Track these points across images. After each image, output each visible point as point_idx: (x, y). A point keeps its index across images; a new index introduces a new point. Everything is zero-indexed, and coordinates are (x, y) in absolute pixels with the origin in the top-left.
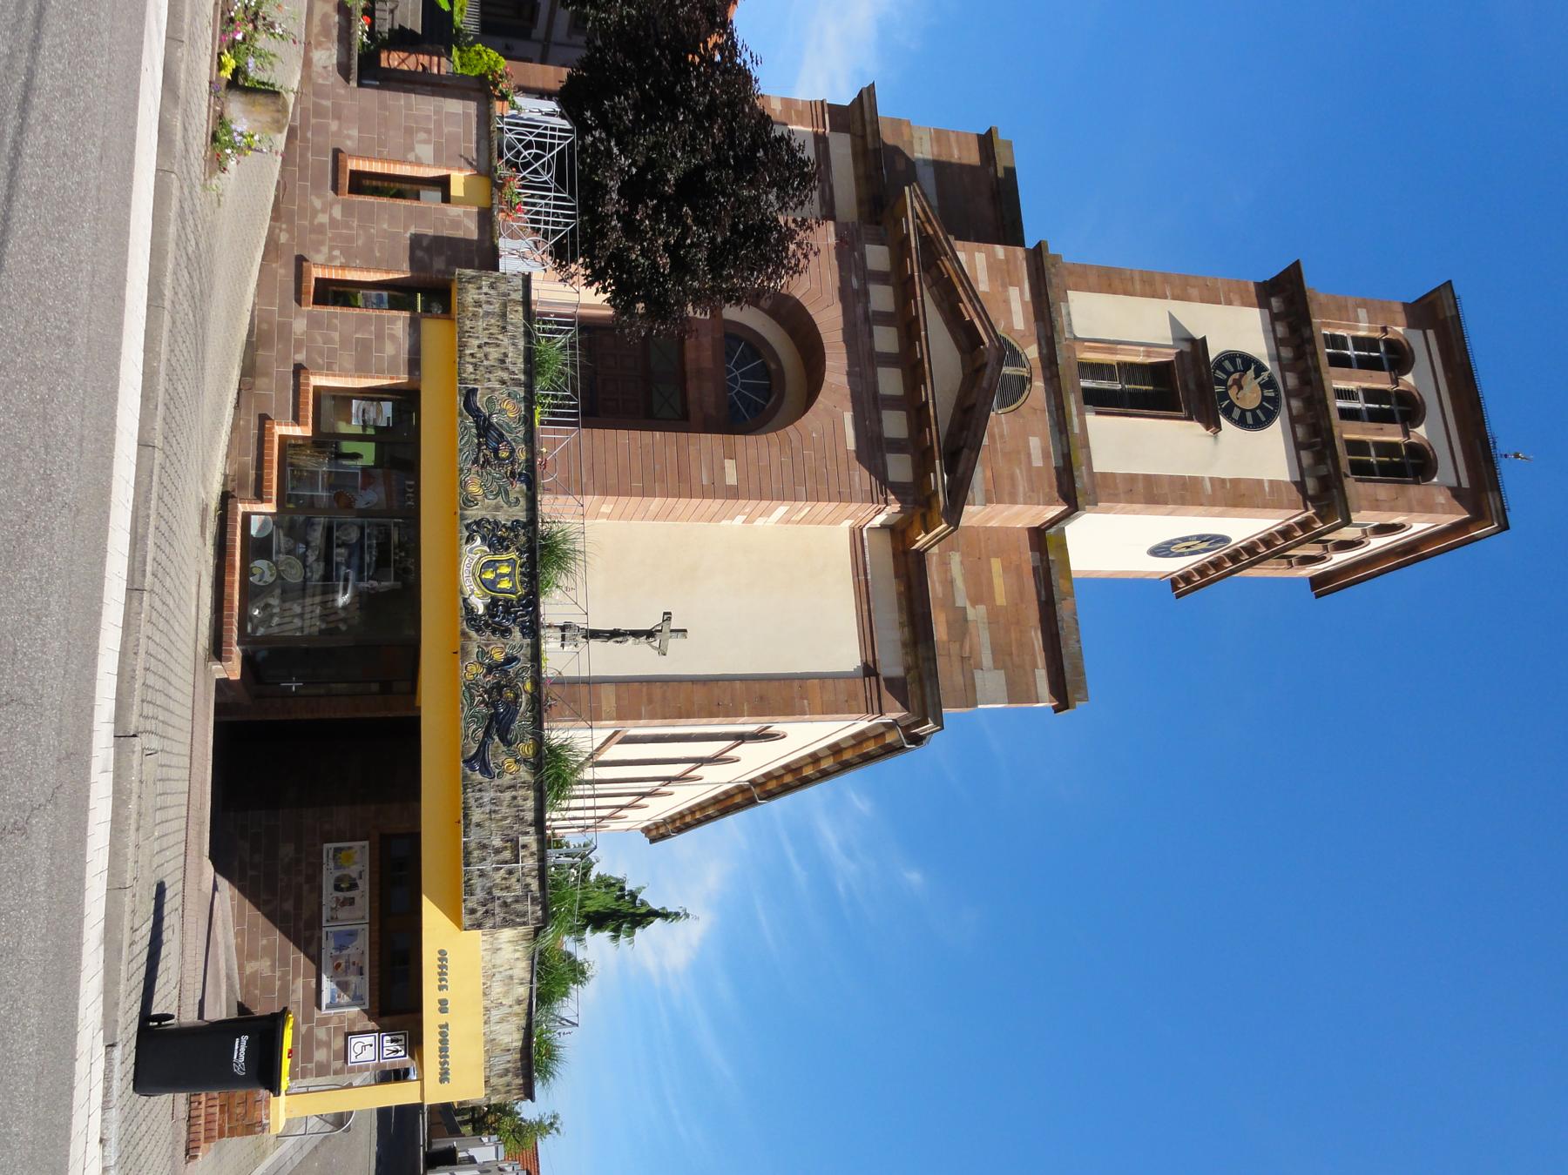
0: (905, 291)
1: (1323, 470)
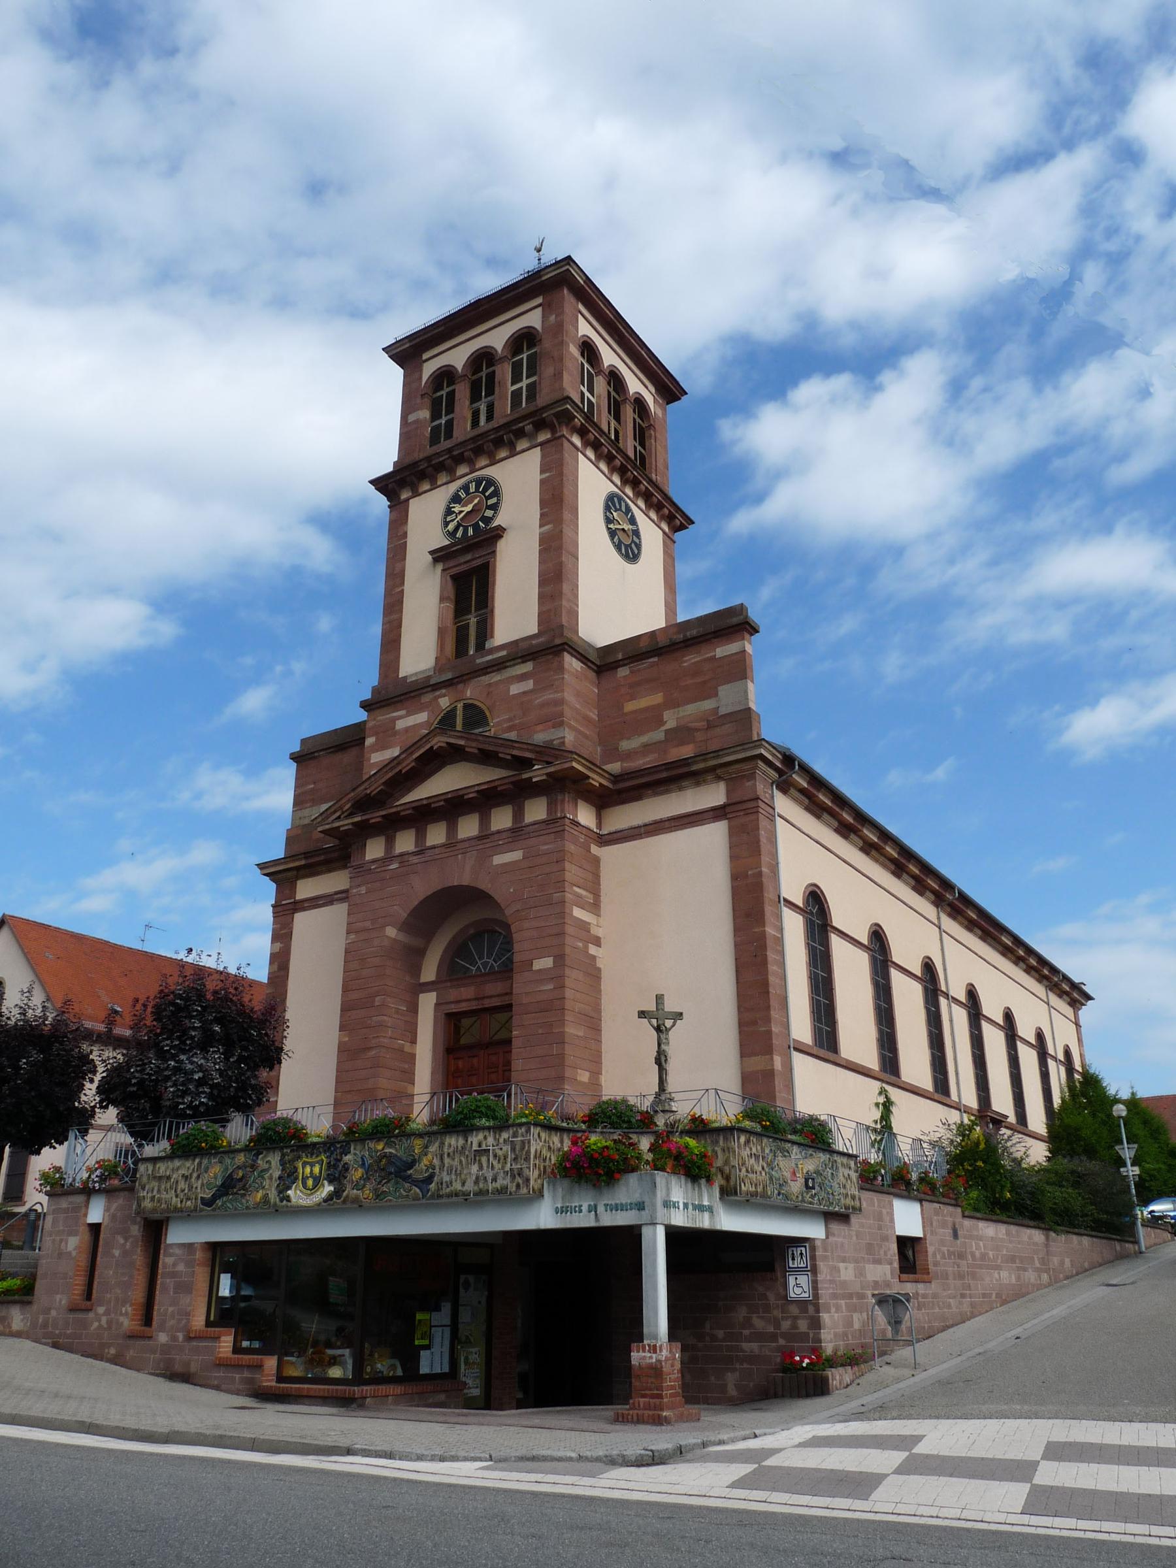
1: (529, 428)
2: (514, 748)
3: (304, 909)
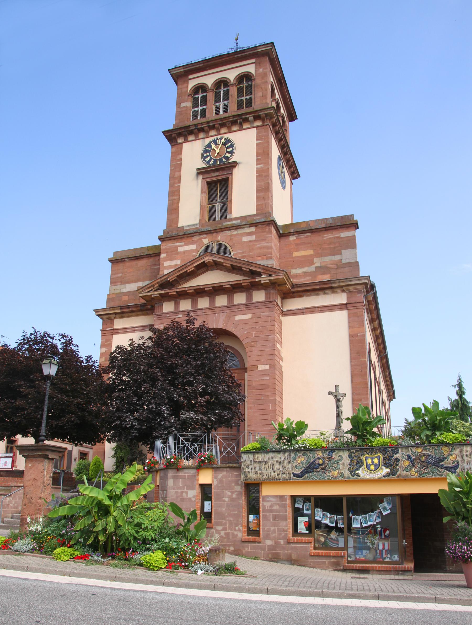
0: (183, 295)
1: (251, 118)
2: (251, 266)
3: (118, 333)
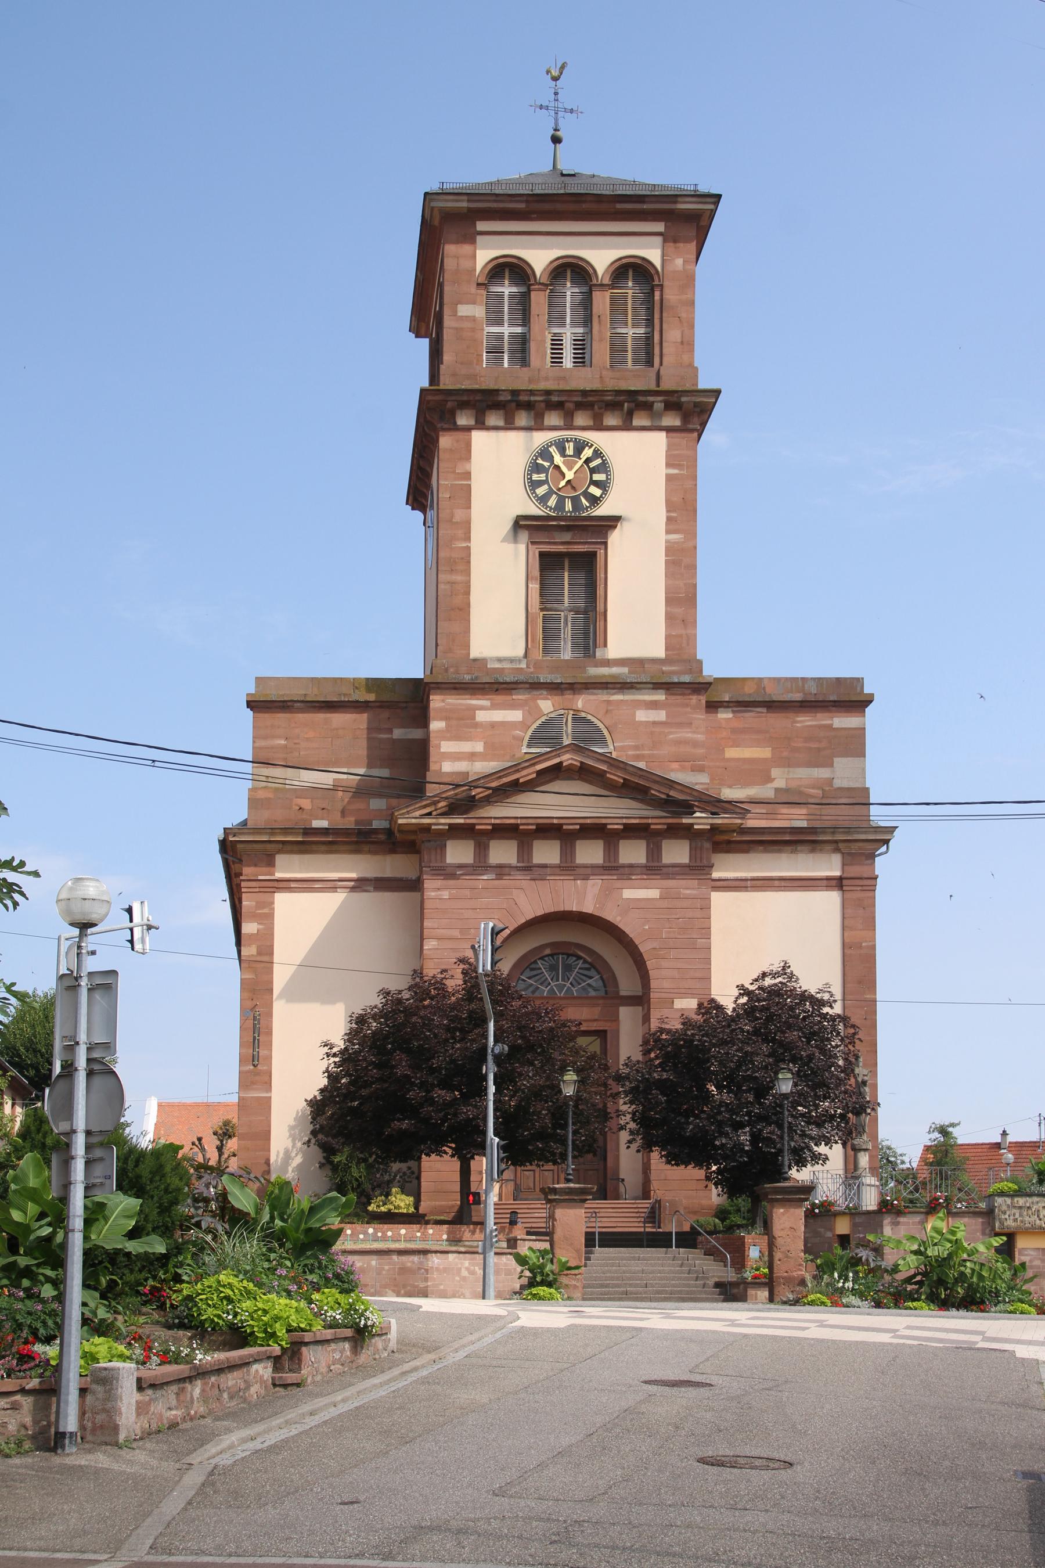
1: (659, 406)
2: (671, 788)
